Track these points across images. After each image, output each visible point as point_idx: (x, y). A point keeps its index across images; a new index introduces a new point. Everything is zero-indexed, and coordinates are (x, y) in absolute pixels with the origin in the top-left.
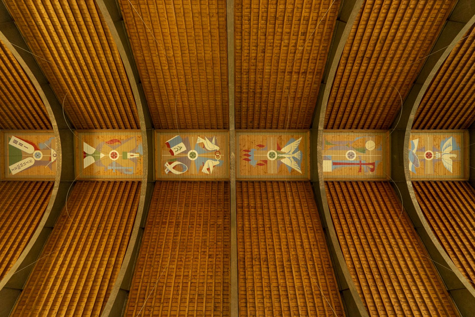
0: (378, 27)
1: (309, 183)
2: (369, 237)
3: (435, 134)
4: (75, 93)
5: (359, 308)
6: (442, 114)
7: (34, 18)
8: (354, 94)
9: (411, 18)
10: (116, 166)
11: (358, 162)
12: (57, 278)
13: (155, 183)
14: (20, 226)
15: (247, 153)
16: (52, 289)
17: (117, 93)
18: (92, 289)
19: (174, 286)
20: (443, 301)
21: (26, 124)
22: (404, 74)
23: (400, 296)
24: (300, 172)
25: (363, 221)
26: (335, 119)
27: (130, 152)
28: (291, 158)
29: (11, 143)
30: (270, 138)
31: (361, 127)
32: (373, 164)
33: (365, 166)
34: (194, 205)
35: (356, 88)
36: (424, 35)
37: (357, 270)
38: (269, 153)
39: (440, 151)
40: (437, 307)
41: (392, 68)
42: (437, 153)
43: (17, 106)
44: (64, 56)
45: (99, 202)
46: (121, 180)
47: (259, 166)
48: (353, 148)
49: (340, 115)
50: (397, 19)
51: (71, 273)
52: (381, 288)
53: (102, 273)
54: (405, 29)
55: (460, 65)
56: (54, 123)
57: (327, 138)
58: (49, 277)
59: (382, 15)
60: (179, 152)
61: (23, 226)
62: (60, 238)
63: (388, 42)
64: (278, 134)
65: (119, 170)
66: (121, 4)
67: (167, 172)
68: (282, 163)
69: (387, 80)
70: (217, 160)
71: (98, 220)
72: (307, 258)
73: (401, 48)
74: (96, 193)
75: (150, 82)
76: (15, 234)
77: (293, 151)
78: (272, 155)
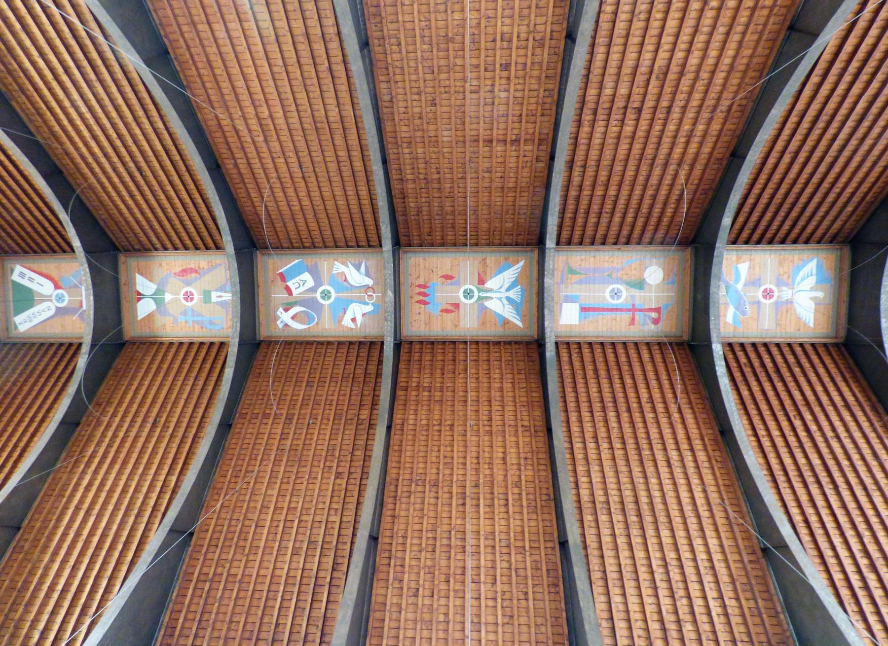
0: (649, 47)
1: (534, 346)
2: (631, 446)
3: (783, 253)
4: (110, 189)
5: (576, 575)
6: (794, 214)
7: (15, 57)
8: (615, 179)
9: (714, 27)
10: (193, 316)
11: (630, 307)
12: (78, 508)
13: (254, 345)
14: (27, 420)
15: (422, 290)
16: (68, 527)
17: (181, 187)
18: (133, 529)
19: (270, 527)
20: (749, 567)
21: (37, 244)
22: (710, 140)
23: (671, 555)
24: (520, 324)
25: (625, 417)
26: (585, 226)
27: (217, 290)
28: (504, 300)
29: (15, 277)
30: (465, 263)
31: (601, 241)
32: (658, 310)
33: (642, 314)
34: (321, 382)
35: (618, 168)
36: (745, 61)
37: (599, 506)
38: (462, 289)
39: (791, 286)
40: (735, 577)
41: (686, 127)
42: (784, 288)
43: (15, 214)
44: (78, 122)
45: (159, 379)
46: (201, 340)
47: (445, 314)
48: (620, 281)
49: (592, 220)
50: (687, 30)
51: (101, 501)
52: (637, 540)
53: (152, 502)
54: (706, 50)
55: (824, 118)
56: (76, 243)
57: (558, 260)
58: (66, 508)
59: (655, 24)
60: (302, 289)
61: (32, 420)
62: (89, 440)
63: (672, 76)
64: (480, 256)
65: (198, 322)
66: (161, 24)
67: (281, 326)
68: (486, 308)
69: (678, 150)
70: (367, 304)
71: (155, 410)
72: (510, 482)
73: (700, 86)
74: (157, 363)
75: (236, 165)
76: (18, 434)
77: (506, 285)
78: (468, 294)
